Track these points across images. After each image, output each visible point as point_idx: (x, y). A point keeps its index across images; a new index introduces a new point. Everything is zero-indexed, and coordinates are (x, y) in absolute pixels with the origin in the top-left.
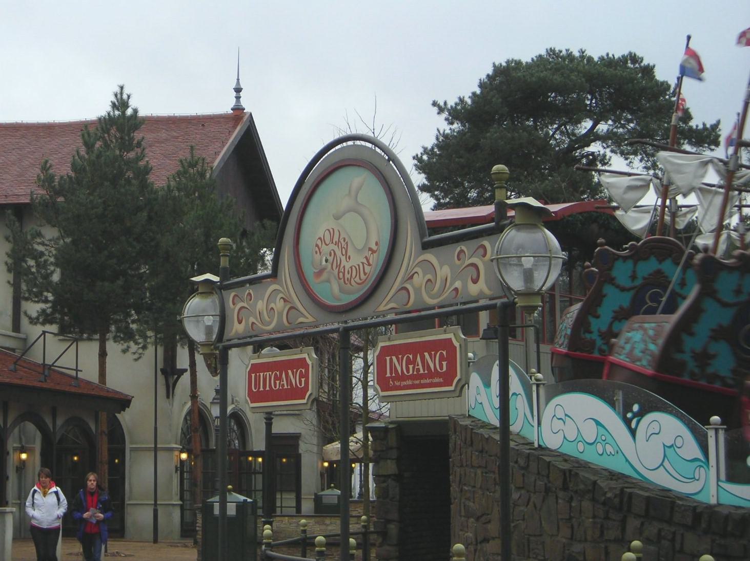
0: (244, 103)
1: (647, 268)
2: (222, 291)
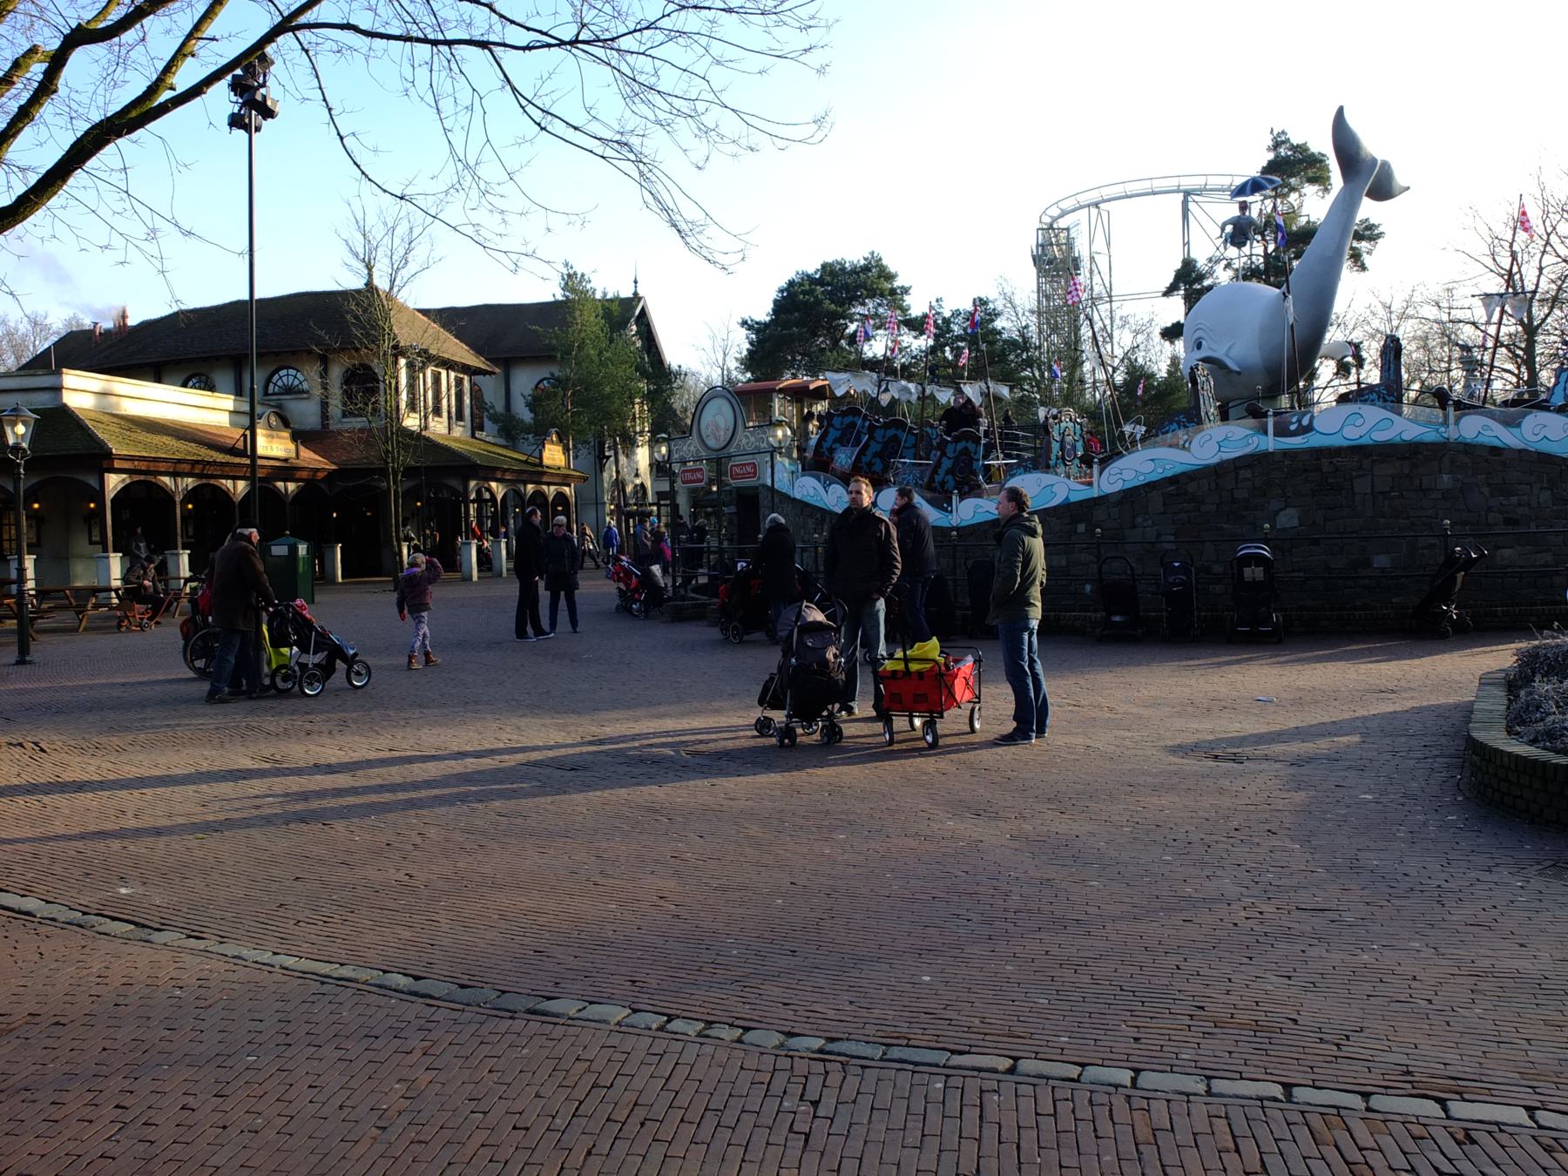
0: (639, 291)
1: (849, 419)
2: (28, 658)
